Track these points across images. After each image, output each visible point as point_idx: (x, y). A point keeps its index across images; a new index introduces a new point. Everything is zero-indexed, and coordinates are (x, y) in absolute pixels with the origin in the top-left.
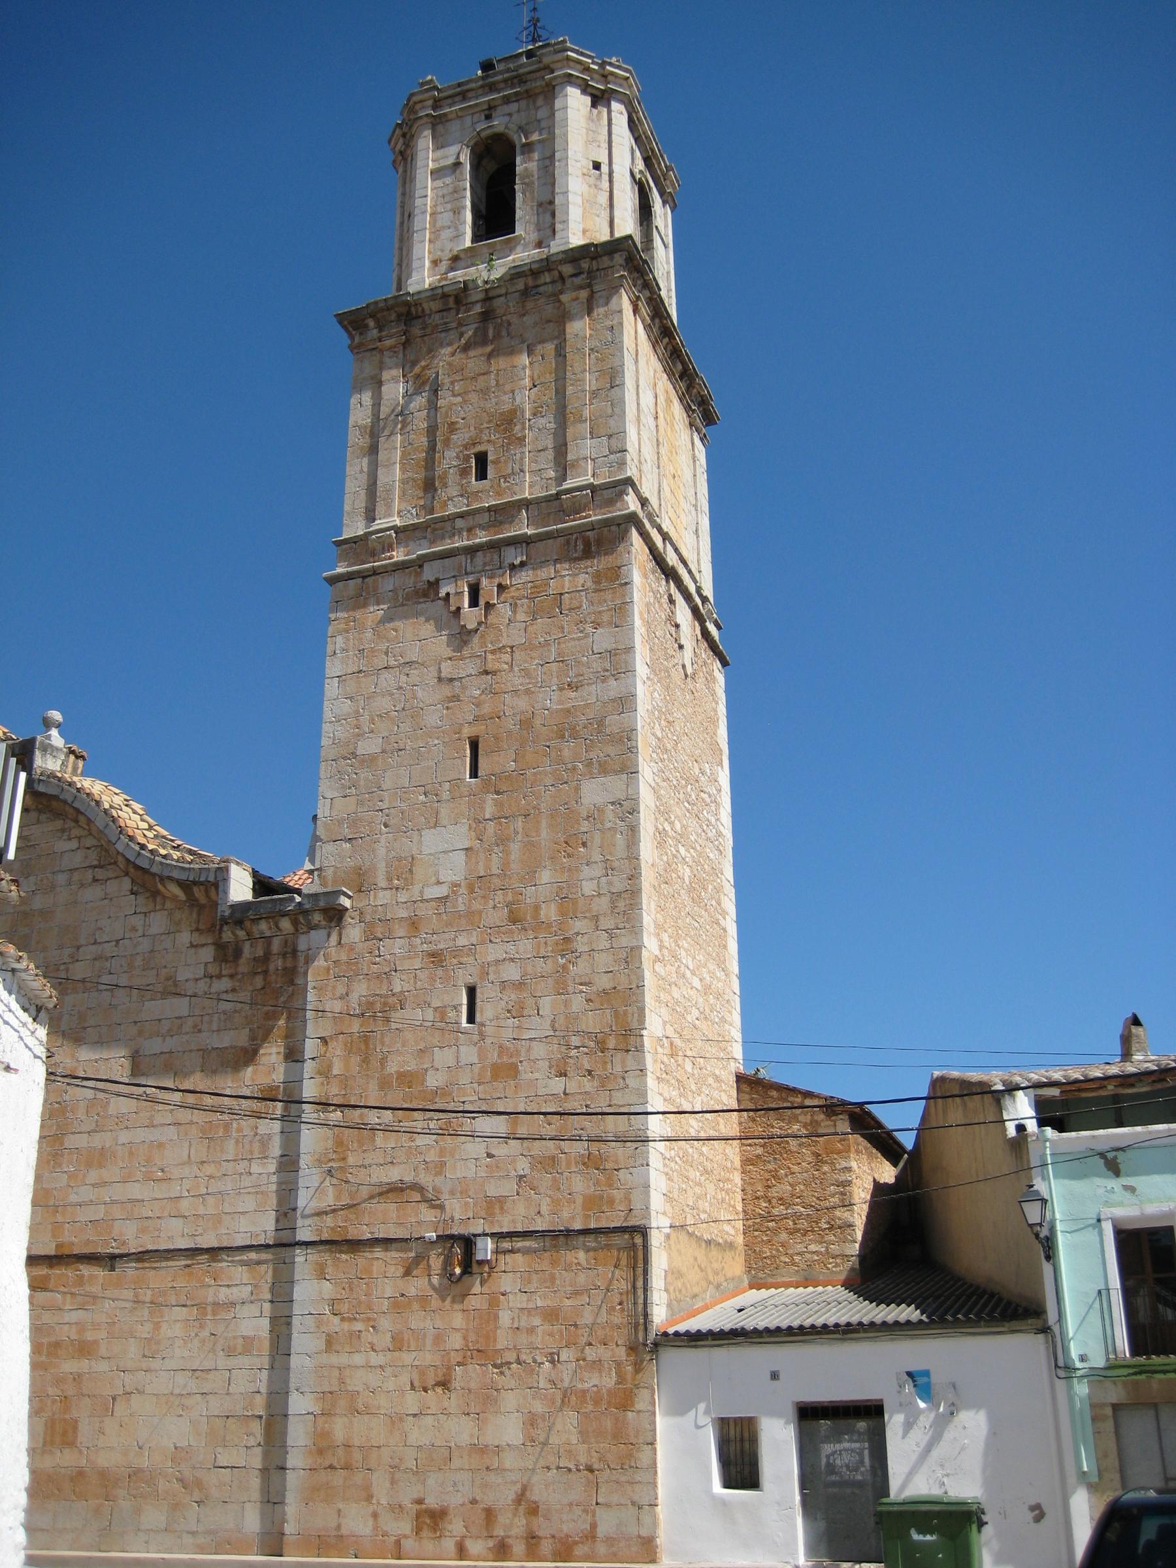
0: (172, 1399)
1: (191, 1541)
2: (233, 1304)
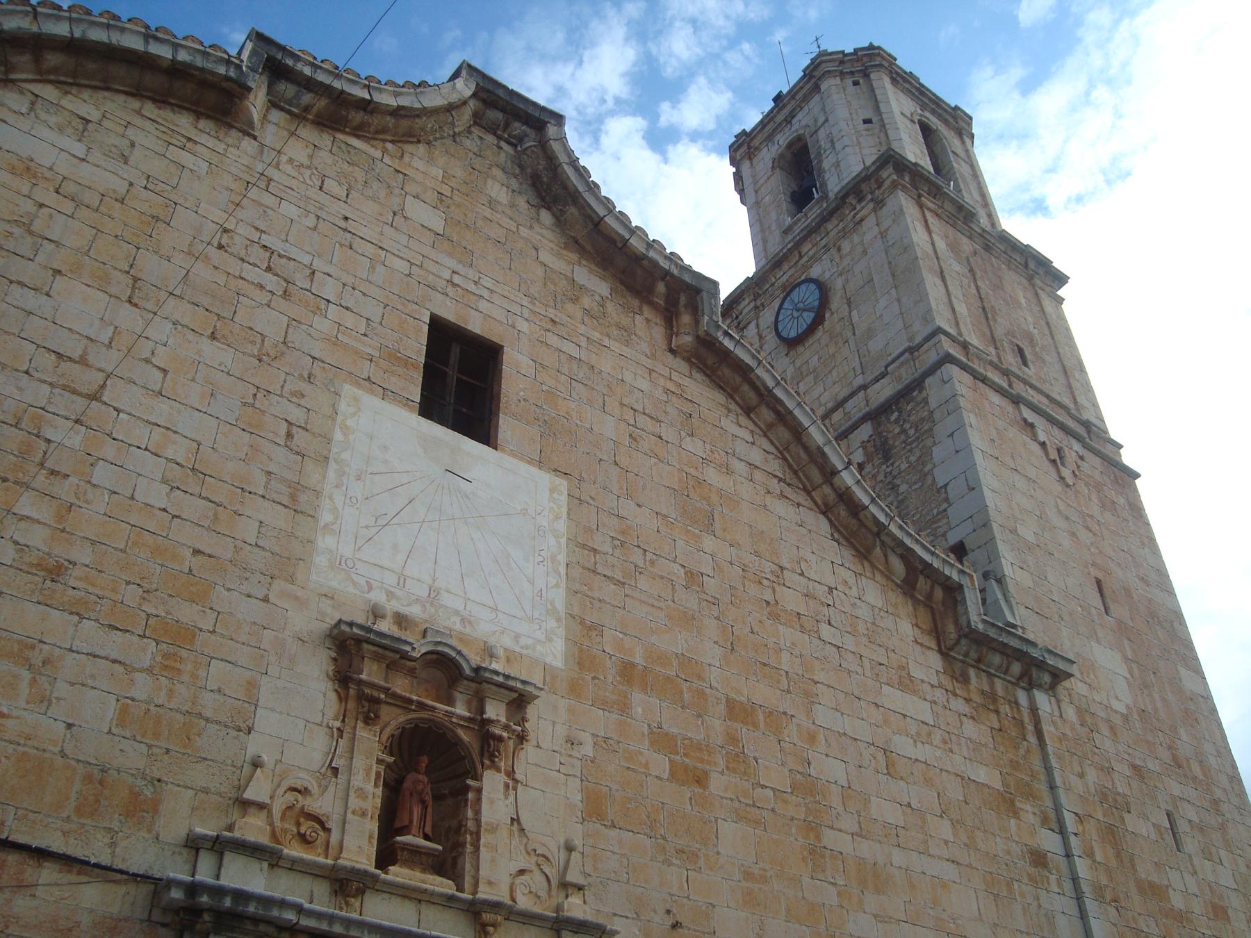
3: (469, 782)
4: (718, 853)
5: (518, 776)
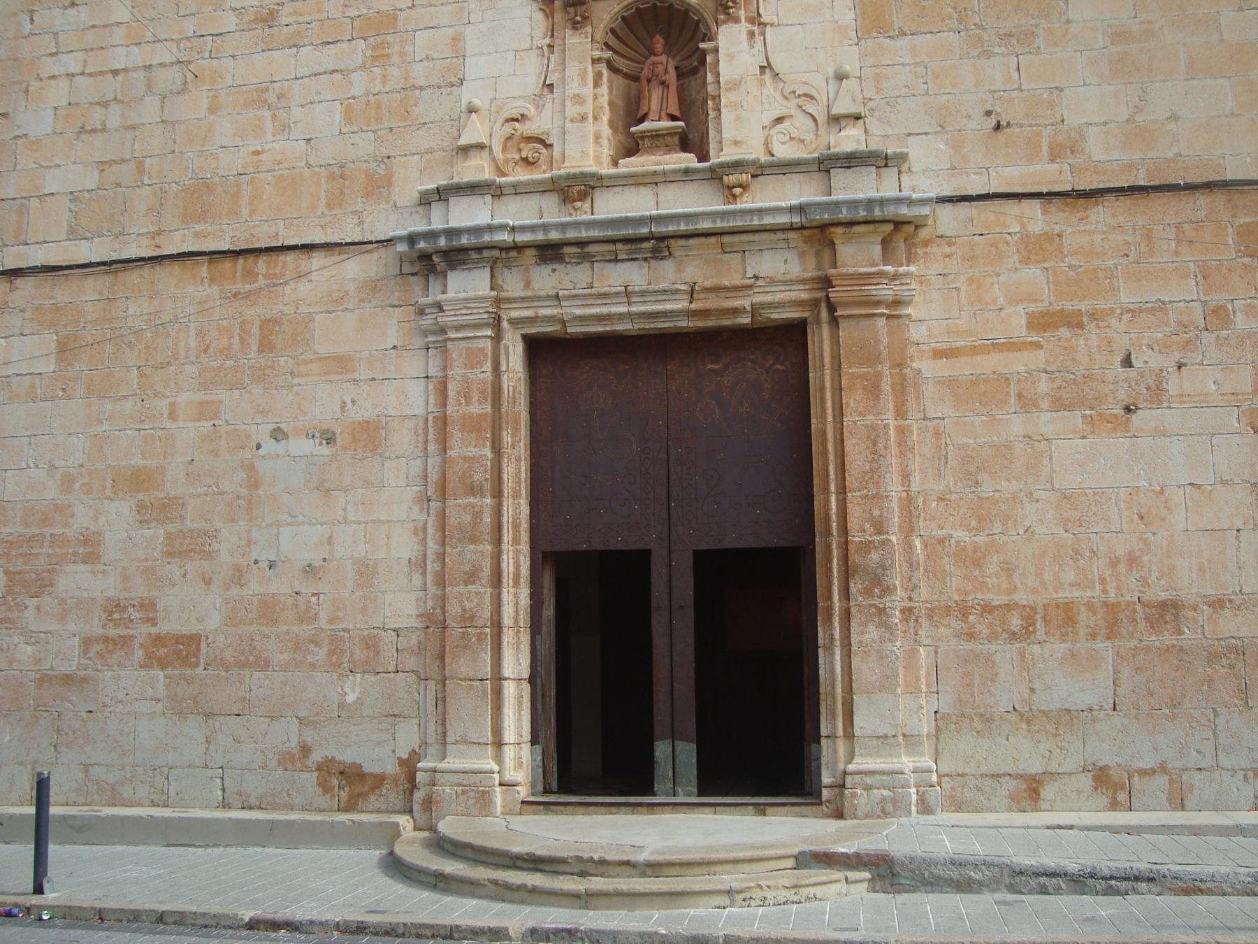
3: (702, 45)
4: (1068, 22)
5: (765, 18)
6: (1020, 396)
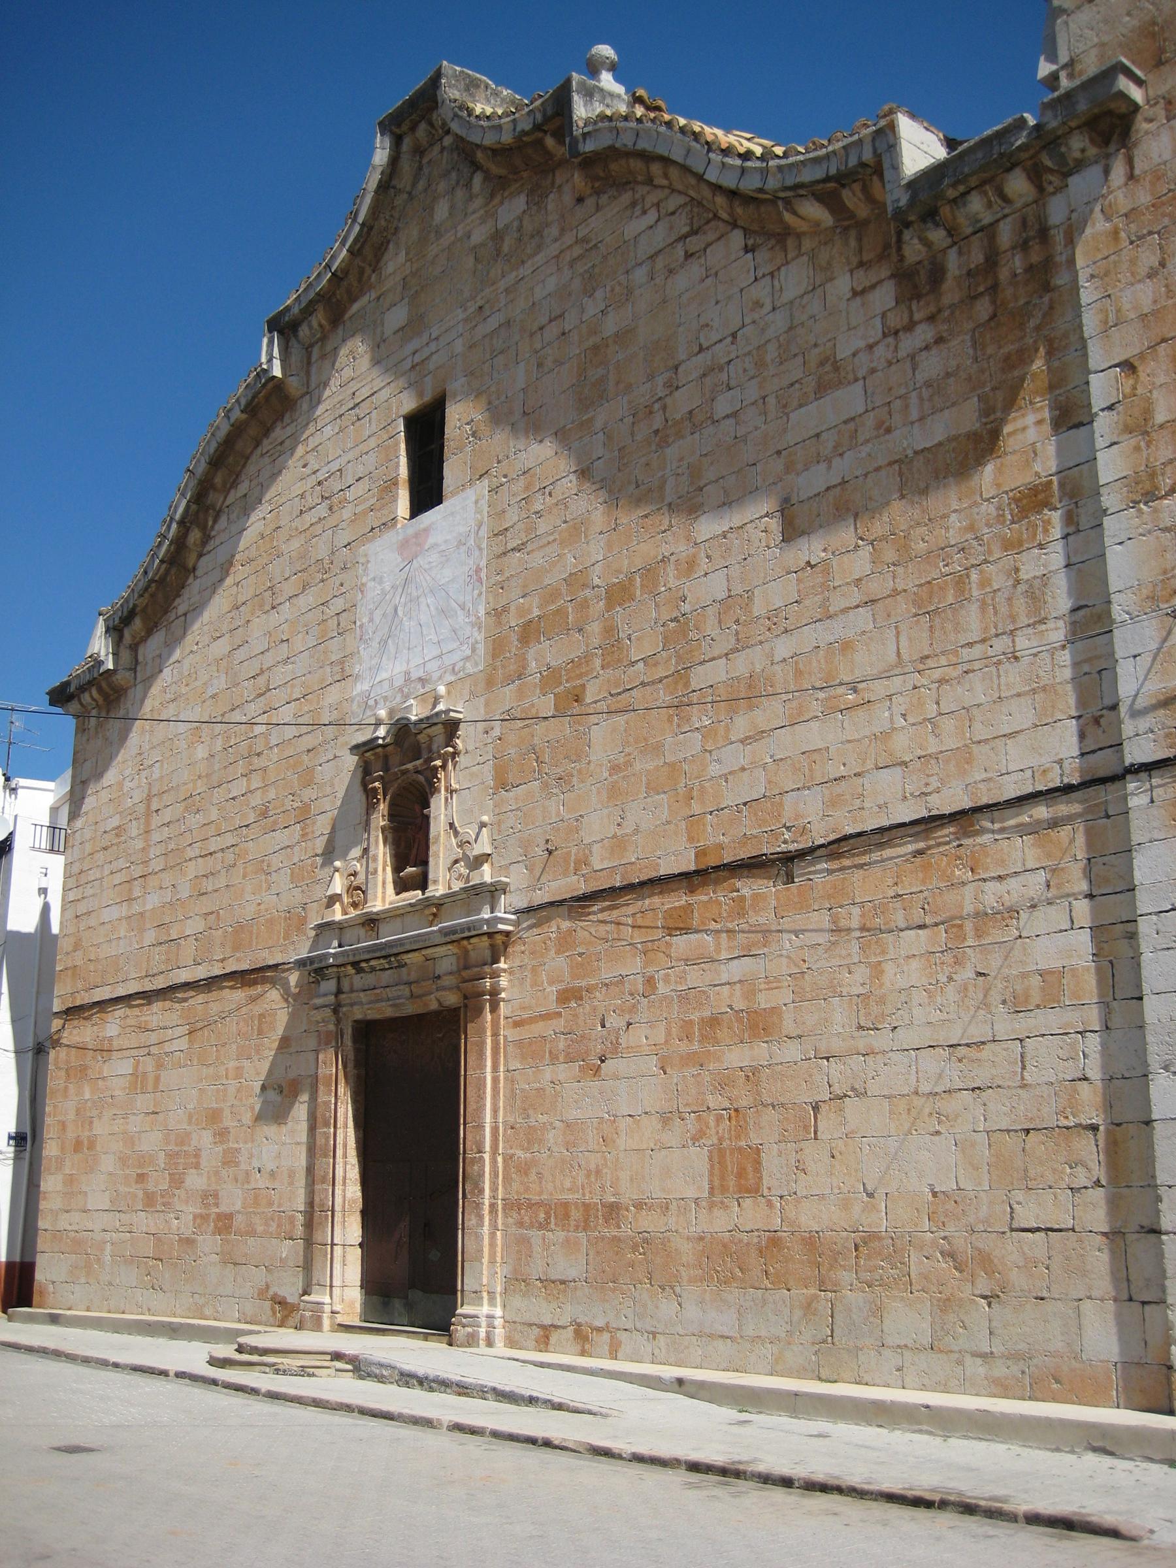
0: (918, 1102)
1: (982, 1371)
2: (1013, 911)
6: (550, 1052)
